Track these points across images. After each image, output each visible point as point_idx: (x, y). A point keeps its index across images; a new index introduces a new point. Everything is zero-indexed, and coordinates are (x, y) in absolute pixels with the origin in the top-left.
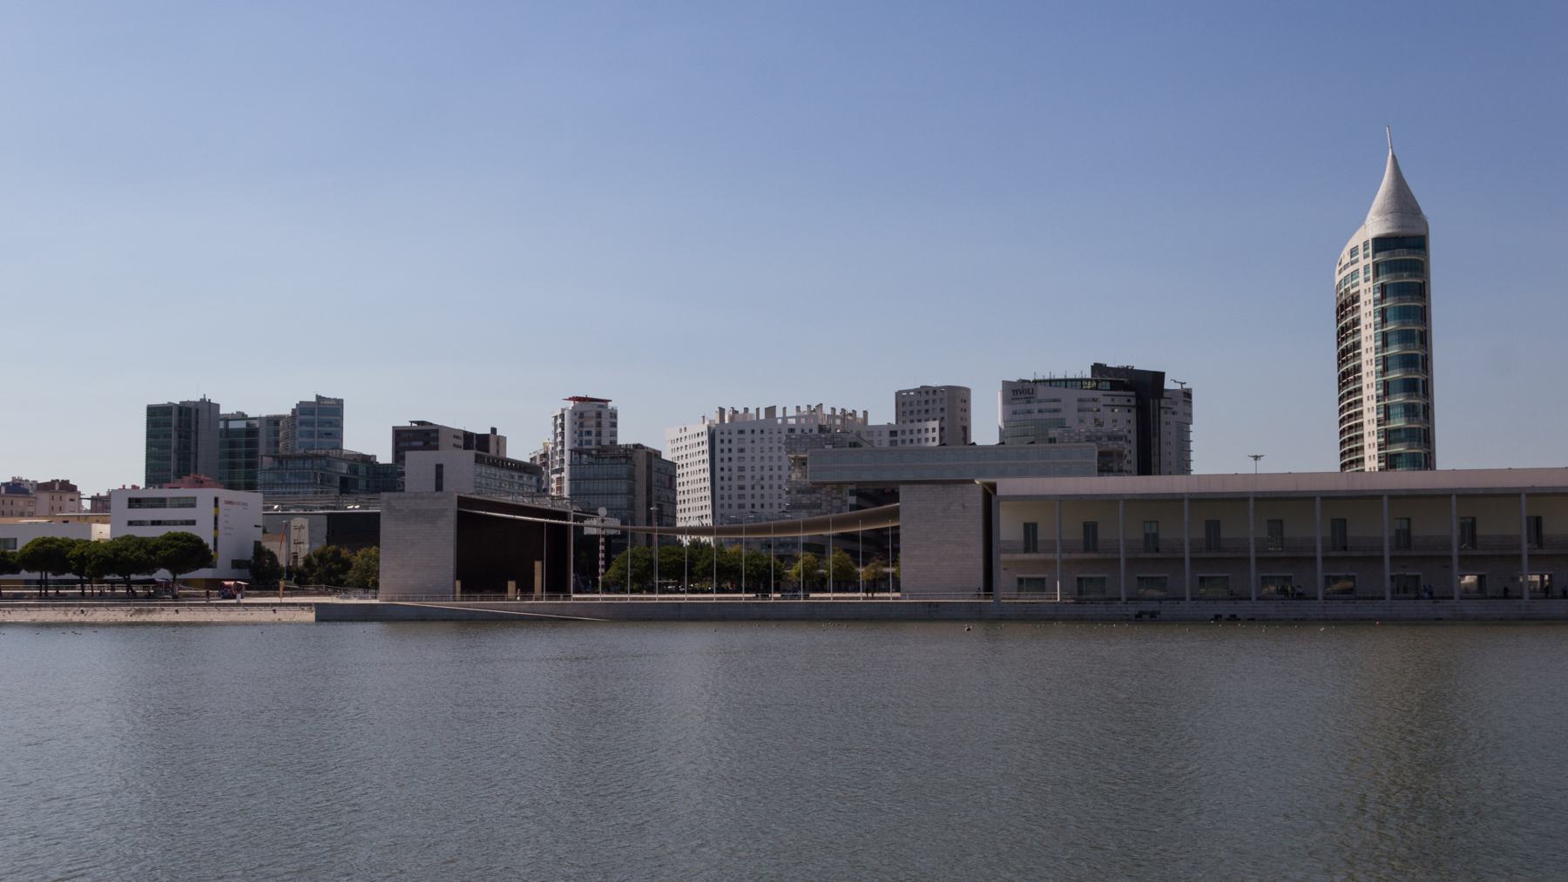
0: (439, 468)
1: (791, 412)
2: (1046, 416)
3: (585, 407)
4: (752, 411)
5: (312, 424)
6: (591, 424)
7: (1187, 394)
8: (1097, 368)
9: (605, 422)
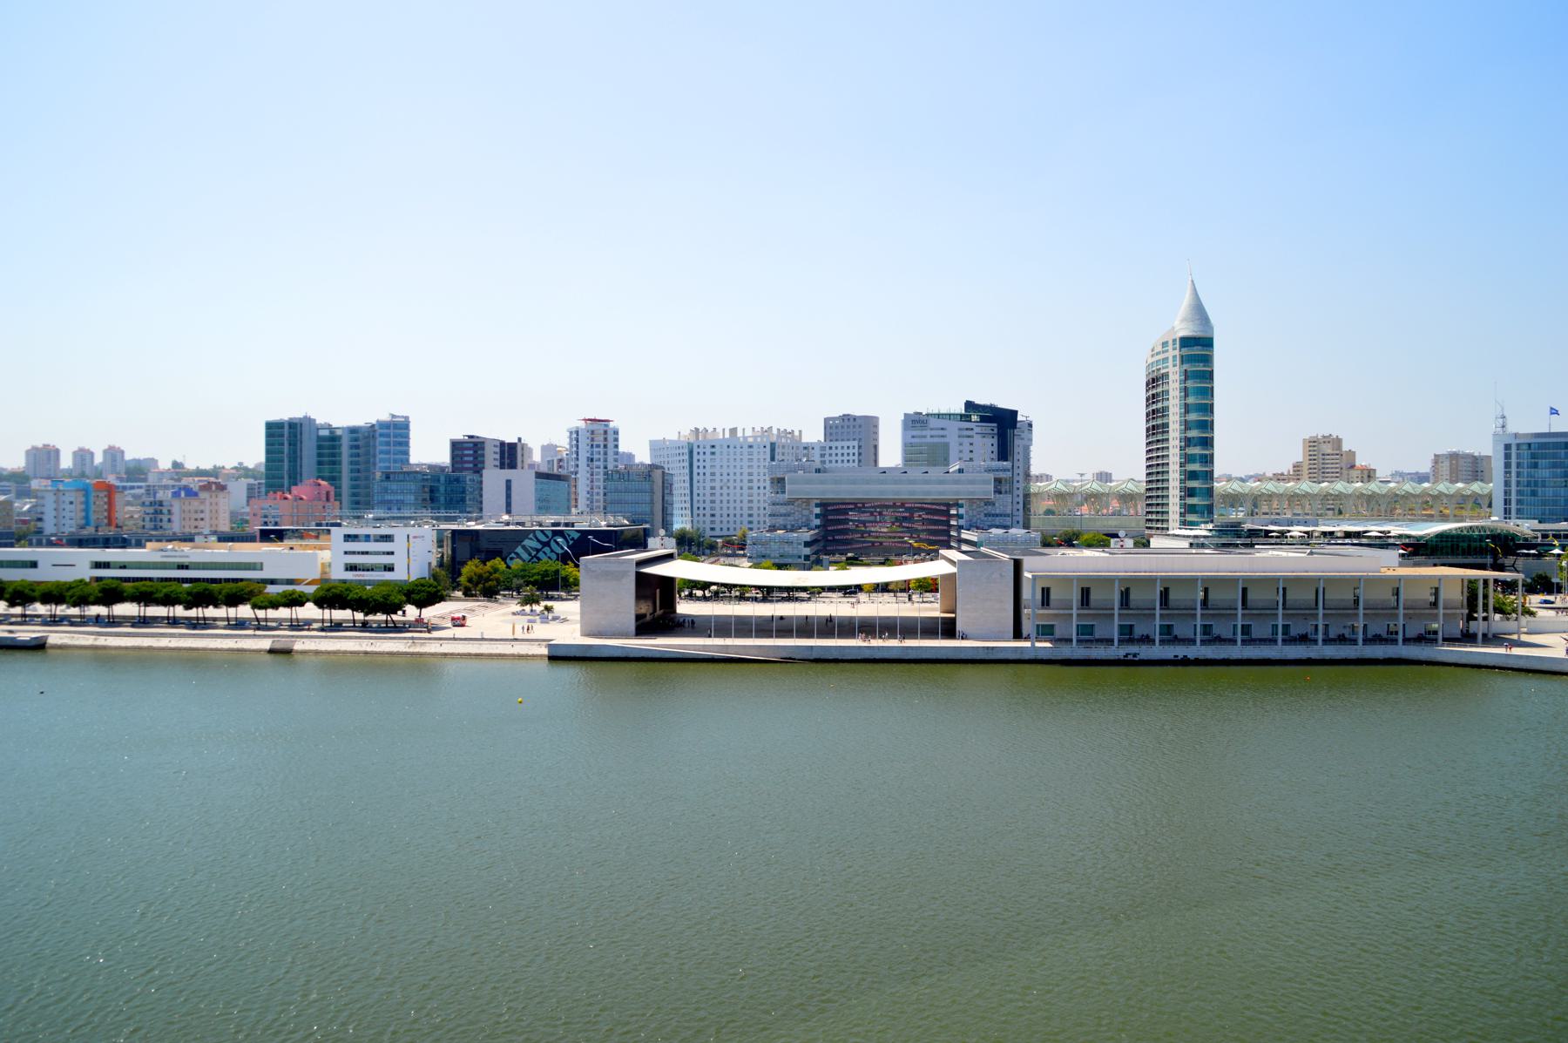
0: (508, 483)
1: (749, 433)
2: (936, 440)
3: (595, 426)
4: (719, 430)
5: (388, 436)
6: (599, 440)
7: (1030, 425)
8: (969, 405)
9: (610, 437)
